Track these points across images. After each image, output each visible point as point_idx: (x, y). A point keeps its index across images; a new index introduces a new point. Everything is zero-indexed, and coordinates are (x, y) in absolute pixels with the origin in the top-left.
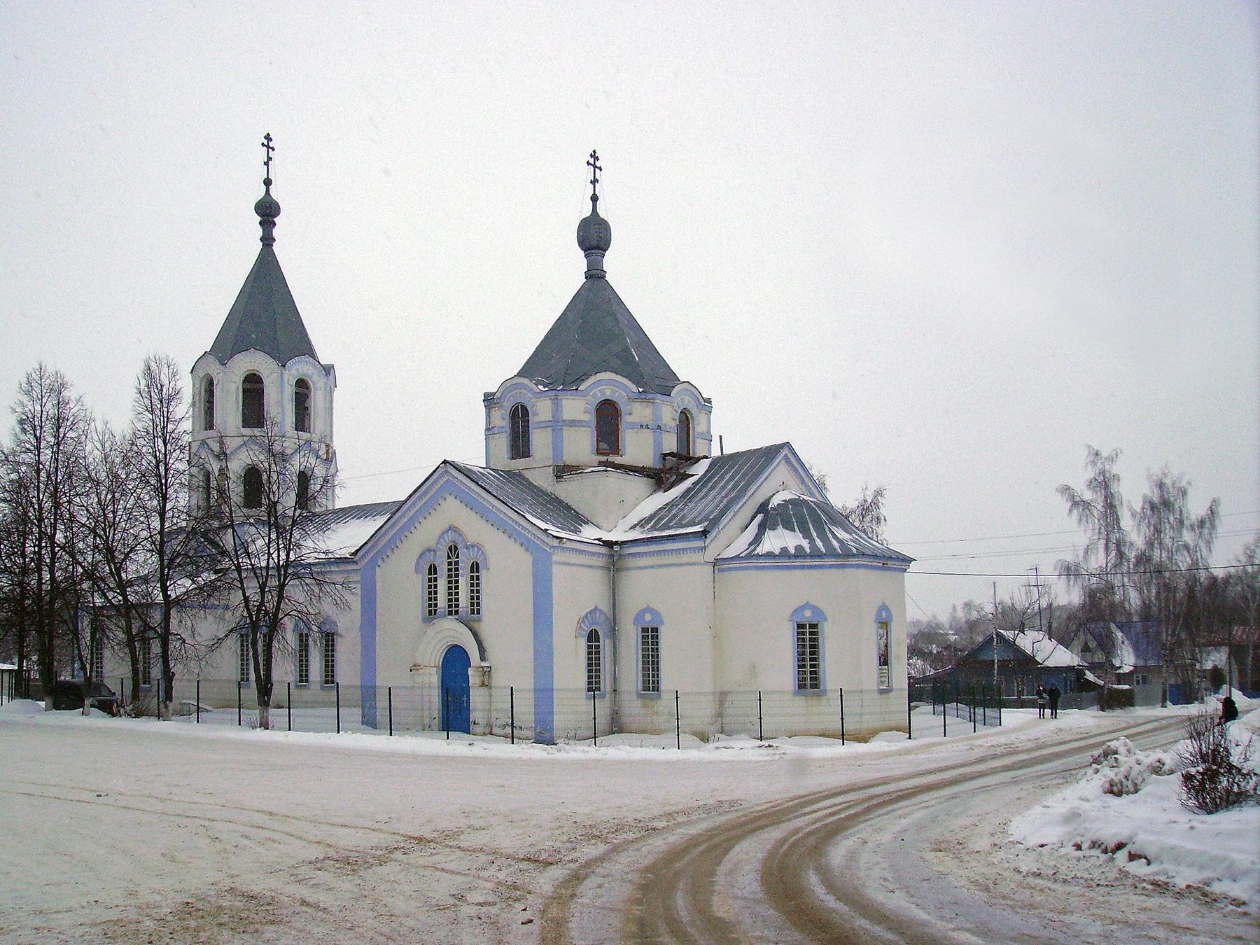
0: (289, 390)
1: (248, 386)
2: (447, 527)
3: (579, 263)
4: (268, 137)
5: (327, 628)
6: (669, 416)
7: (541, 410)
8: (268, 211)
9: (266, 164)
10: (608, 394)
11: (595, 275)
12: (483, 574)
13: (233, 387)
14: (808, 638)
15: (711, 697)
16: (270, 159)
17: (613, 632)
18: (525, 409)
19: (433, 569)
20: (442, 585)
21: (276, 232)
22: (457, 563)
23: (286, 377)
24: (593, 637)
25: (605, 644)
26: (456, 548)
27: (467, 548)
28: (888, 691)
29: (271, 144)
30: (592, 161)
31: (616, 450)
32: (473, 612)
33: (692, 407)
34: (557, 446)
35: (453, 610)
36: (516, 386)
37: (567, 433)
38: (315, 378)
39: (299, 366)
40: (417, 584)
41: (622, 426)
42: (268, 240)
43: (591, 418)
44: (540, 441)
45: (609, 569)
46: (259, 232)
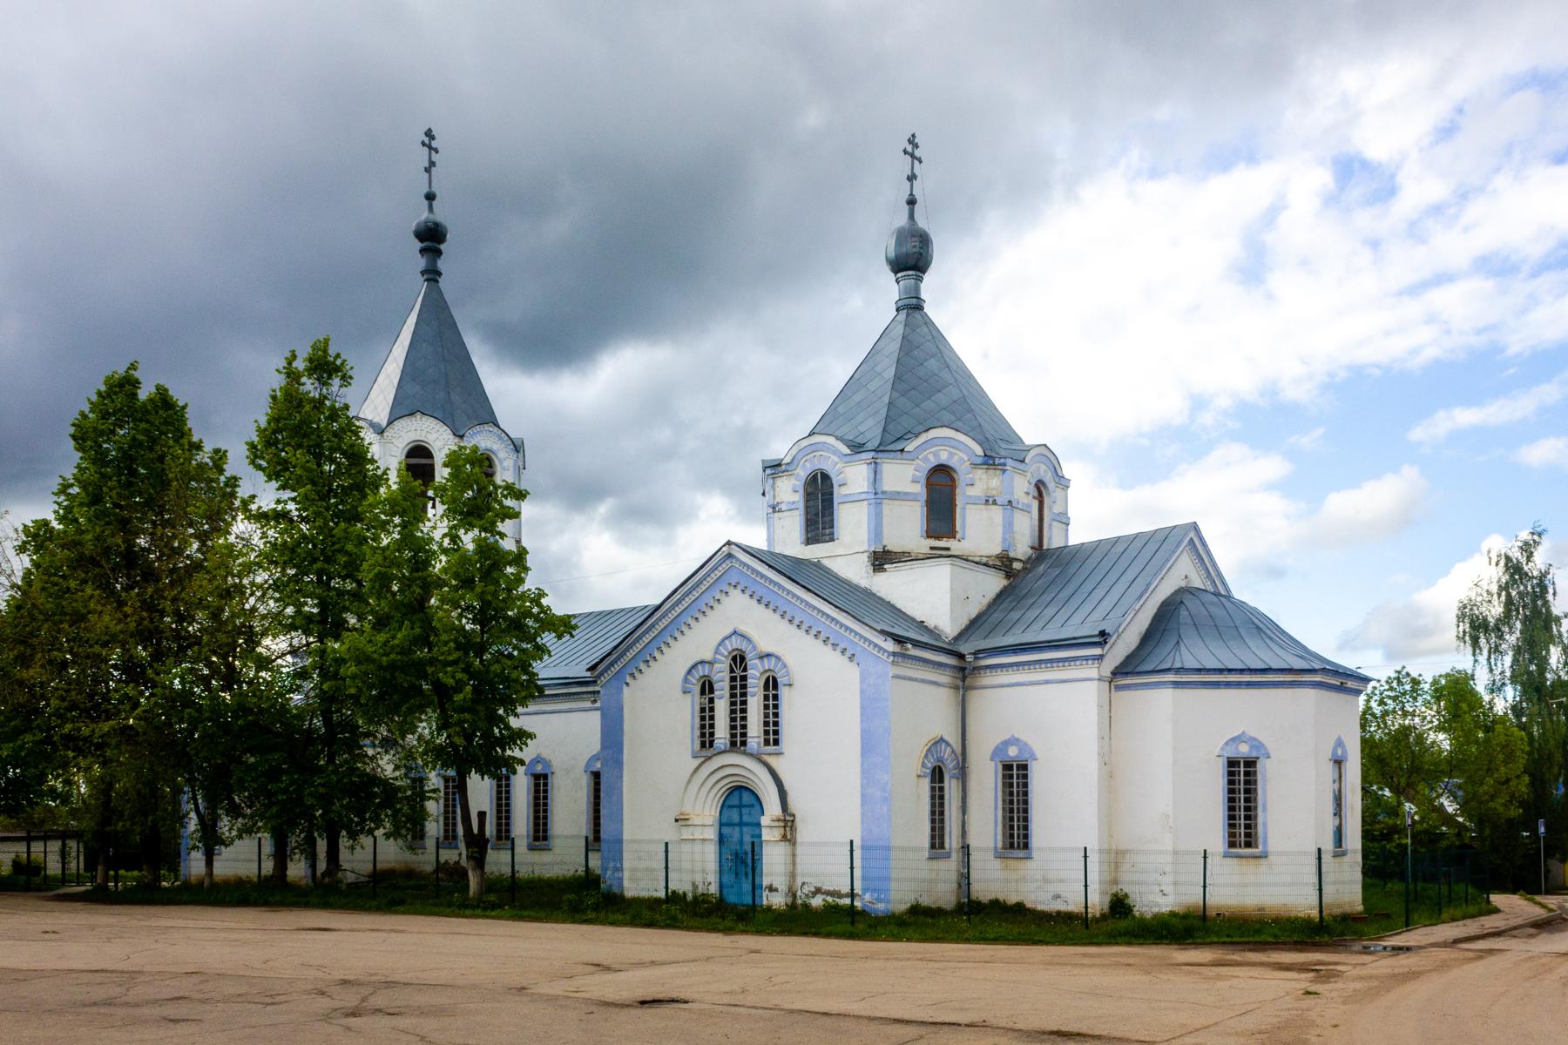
1: (413, 461)
2: (729, 631)
4: (429, 134)
5: (539, 769)
6: (1021, 488)
7: (853, 478)
9: (428, 170)
10: (944, 458)
12: (784, 692)
14: (1242, 778)
16: (432, 164)
17: (963, 773)
18: (826, 477)
19: (707, 688)
20: (722, 708)
21: (441, 264)
22: (744, 678)
24: (937, 775)
25: (951, 788)
26: (743, 659)
27: (761, 658)
28: (1344, 854)
29: (434, 144)
30: (909, 149)
32: (767, 742)
33: (1048, 478)
34: (877, 530)
35: (738, 741)
36: (814, 448)
37: (889, 508)
38: (502, 455)
40: (685, 711)
41: (959, 501)
43: (920, 489)
44: (852, 522)
45: (956, 688)
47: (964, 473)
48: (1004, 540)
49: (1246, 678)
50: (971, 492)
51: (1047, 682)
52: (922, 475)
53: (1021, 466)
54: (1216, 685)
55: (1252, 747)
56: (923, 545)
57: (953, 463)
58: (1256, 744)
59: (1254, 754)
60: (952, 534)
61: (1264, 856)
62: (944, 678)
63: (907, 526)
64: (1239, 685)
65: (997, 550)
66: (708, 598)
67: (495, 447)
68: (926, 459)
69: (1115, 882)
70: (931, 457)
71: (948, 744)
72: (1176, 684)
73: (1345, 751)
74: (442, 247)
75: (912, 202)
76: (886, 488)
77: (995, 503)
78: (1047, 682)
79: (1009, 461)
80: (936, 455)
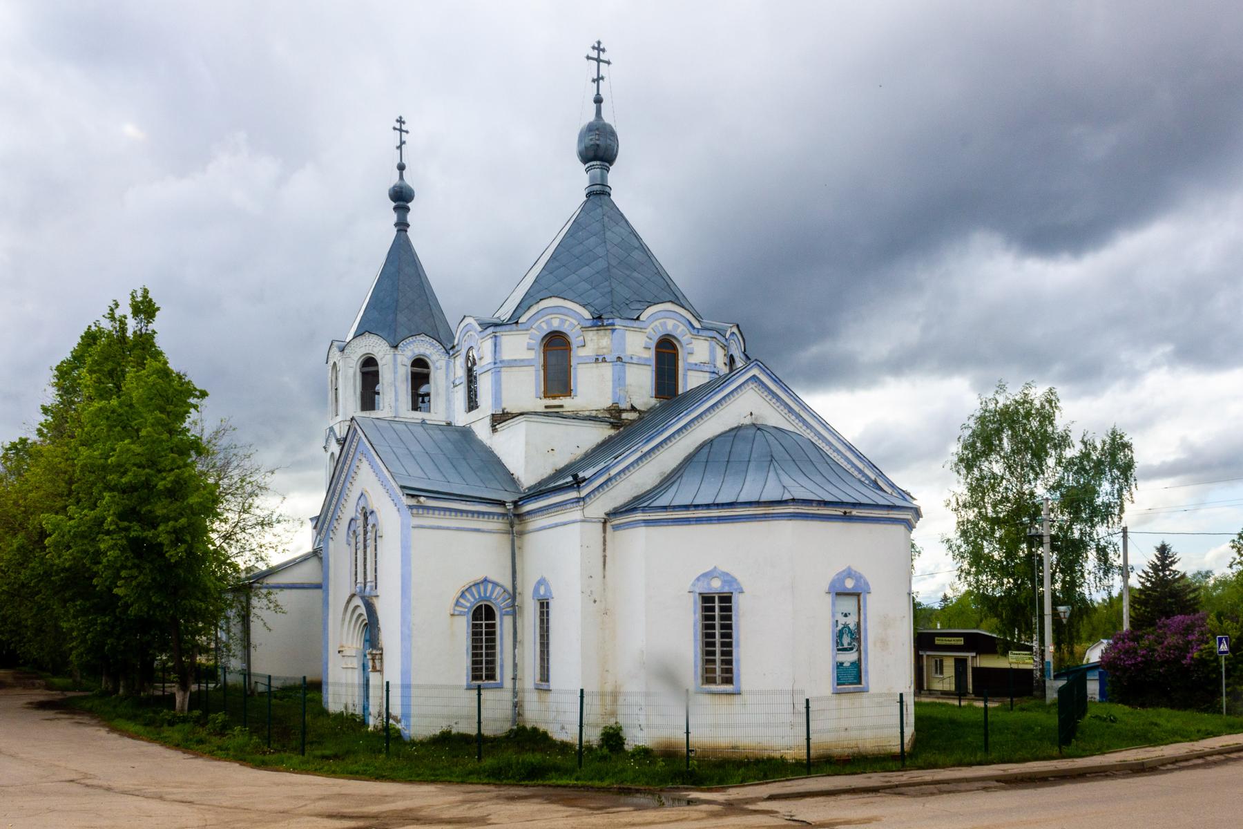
0: (404, 371)
3: (580, 178)
8: (401, 197)
9: (400, 147)
10: (556, 325)
11: (599, 193)
13: (351, 371)
14: (717, 615)
15: (358, 711)
21: (410, 218)
23: (399, 358)
31: (567, 391)
37: (506, 374)
38: (434, 358)
39: (411, 347)
42: (402, 226)
43: (651, 355)
45: (507, 532)
46: (394, 217)
47: (575, 338)
48: (614, 393)
49: (715, 513)
50: (582, 353)
51: (556, 525)
52: (653, 345)
53: (636, 324)
54: (687, 521)
55: (724, 582)
56: (540, 404)
57: (565, 328)
58: (728, 579)
59: (726, 589)
60: (567, 391)
61: (738, 693)
62: (497, 525)
63: (523, 389)
64: (709, 520)
65: (608, 403)
66: (353, 467)
67: (428, 352)
68: (540, 328)
69: (613, 714)
70: (544, 326)
71: (495, 584)
72: (647, 523)
73: (548, 589)
74: (410, 205)
75: (598, 101)
76: (505, 357)
77: (604, 360)
78: (556, 525)
79: (617, 321)
80: (548, 322)
